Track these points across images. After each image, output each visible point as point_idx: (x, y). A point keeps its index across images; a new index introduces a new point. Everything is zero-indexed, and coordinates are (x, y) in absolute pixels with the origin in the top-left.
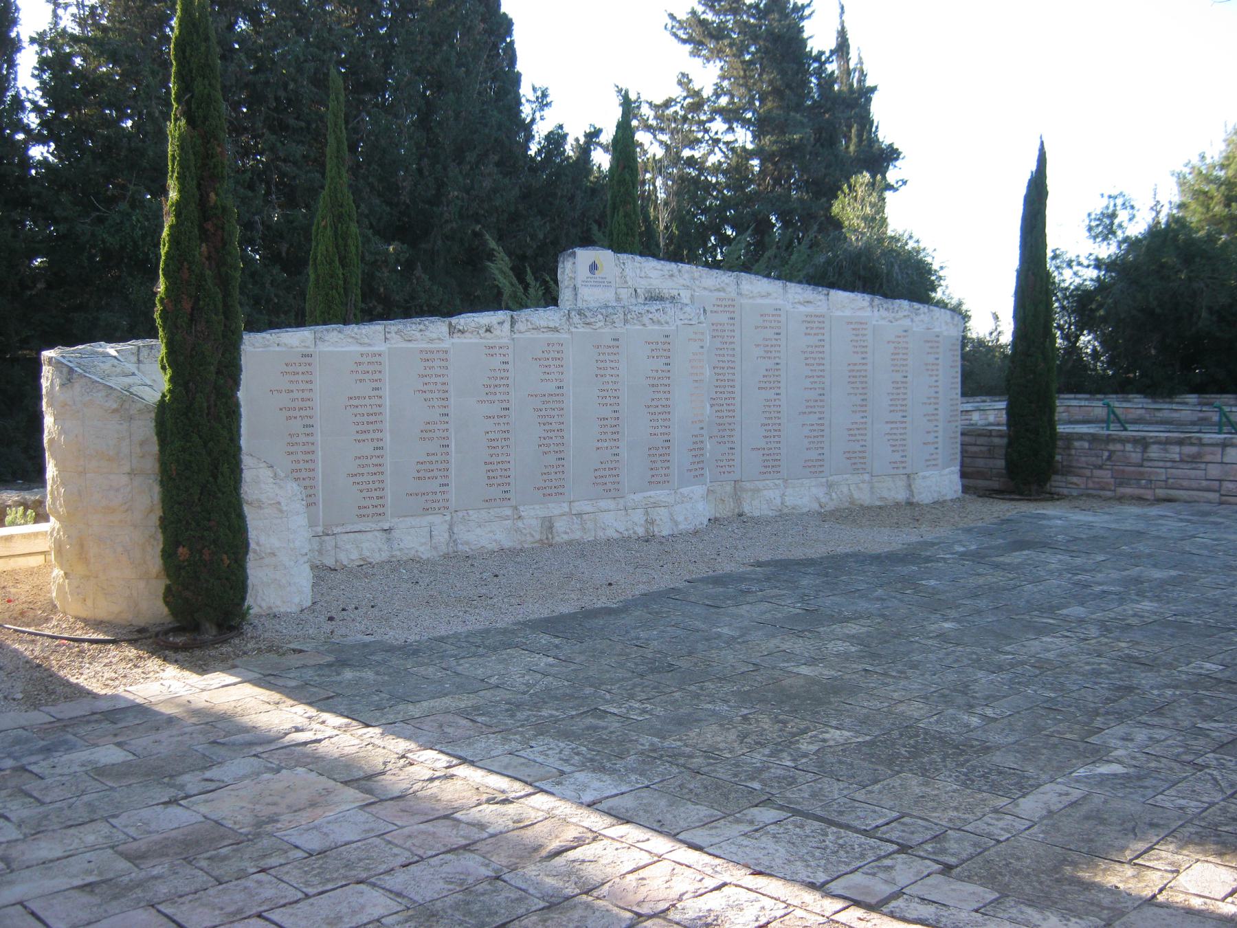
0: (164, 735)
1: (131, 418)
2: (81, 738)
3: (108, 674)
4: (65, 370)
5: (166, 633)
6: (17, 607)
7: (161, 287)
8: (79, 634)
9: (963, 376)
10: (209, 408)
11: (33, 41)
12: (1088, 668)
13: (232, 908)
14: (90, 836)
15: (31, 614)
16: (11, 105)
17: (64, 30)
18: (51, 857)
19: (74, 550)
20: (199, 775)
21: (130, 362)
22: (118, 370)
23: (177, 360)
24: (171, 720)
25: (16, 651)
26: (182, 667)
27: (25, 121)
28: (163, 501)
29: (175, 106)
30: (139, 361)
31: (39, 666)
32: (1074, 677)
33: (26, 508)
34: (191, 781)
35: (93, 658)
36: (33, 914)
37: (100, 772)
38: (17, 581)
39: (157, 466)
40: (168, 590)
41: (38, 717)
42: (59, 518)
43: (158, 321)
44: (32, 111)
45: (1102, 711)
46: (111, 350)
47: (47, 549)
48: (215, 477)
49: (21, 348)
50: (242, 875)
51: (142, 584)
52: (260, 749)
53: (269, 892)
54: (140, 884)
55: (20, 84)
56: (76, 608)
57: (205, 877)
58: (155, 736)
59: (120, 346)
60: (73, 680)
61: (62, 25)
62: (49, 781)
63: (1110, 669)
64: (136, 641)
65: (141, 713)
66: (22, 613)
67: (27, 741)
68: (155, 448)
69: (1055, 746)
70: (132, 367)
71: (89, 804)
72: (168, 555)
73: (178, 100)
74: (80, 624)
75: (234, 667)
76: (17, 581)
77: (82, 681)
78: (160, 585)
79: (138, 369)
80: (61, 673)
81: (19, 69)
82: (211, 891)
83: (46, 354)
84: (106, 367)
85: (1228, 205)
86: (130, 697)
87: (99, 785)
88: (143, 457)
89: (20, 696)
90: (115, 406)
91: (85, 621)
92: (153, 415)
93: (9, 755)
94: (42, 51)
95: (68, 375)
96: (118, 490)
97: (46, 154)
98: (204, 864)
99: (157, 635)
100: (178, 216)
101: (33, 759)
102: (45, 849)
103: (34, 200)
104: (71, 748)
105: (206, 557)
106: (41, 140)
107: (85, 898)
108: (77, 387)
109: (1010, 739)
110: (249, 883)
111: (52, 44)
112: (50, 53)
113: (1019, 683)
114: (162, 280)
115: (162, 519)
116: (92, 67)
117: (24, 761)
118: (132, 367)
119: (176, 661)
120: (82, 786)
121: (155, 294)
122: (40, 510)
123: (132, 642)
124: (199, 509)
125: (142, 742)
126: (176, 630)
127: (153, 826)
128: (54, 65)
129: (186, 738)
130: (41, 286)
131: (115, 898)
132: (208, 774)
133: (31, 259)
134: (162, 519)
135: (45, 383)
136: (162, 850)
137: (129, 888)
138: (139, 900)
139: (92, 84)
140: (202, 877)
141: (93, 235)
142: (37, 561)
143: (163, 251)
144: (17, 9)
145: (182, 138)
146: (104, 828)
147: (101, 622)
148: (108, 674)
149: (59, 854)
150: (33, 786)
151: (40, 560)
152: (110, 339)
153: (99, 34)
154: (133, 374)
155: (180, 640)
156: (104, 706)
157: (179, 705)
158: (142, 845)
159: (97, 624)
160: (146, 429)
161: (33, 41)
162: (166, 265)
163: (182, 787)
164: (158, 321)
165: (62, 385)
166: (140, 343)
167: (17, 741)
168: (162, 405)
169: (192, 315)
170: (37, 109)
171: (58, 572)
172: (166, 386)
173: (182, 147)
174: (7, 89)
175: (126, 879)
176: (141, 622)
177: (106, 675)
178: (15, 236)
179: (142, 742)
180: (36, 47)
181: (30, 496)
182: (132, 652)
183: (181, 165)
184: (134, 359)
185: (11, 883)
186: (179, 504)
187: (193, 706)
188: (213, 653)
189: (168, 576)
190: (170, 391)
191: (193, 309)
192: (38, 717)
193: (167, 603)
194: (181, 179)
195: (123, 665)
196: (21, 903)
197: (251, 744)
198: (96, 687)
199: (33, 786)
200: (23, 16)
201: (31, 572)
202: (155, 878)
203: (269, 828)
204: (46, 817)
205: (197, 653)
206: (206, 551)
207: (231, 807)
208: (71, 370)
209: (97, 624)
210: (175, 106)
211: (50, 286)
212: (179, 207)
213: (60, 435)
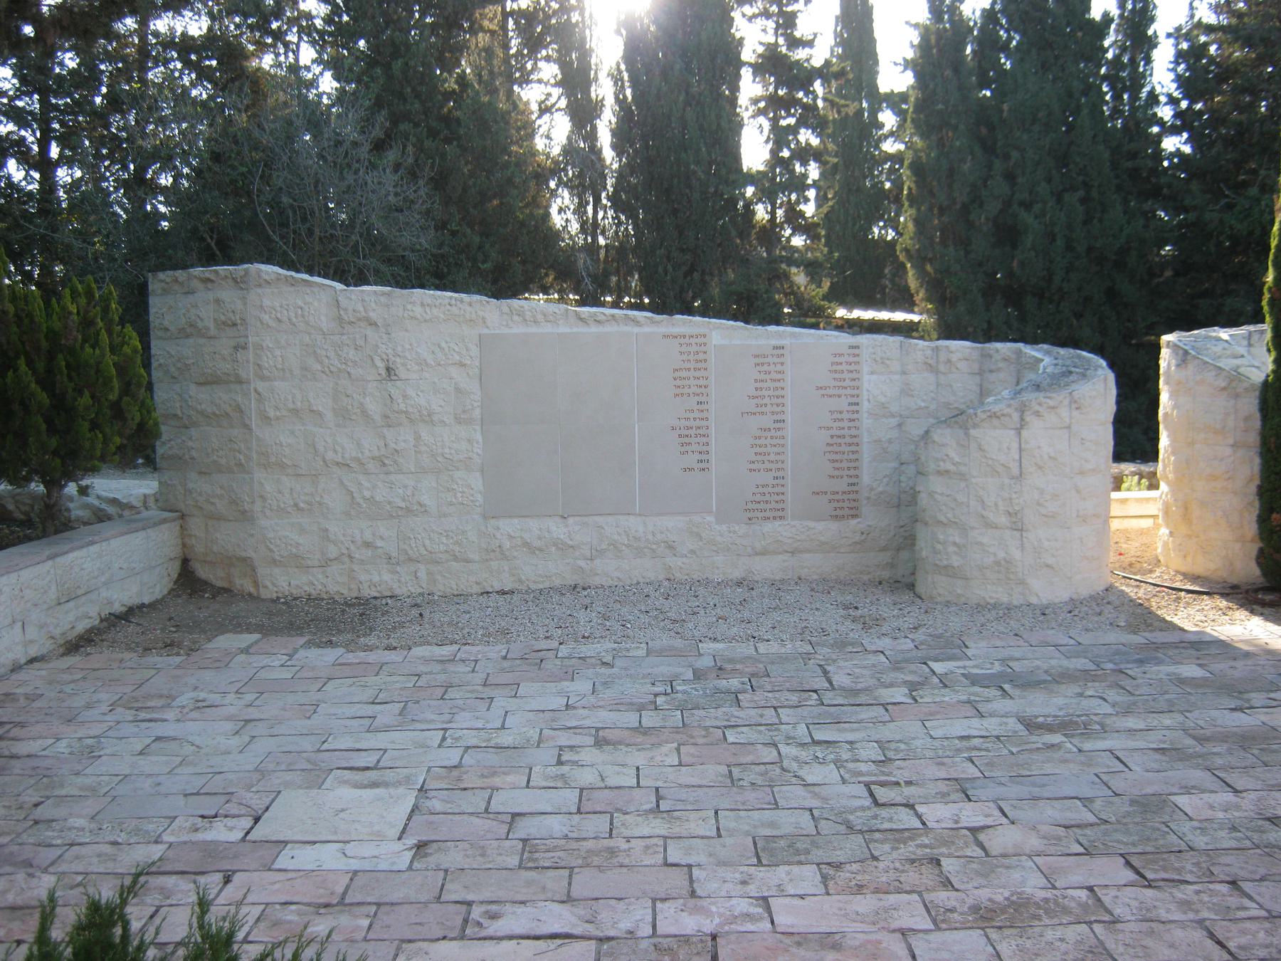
0: (1239, 664)
1: (1237, 396)
3: (1199, 617)
4: (1181, 352)
5: (1257, 591)
6: (1126, 560)
11: (1169, 35)
14: (1167, 721)
16: (1146, 100)
17: (1200, 22)
18: (1135, 727)
19: (1181, 513)
20: (1265, 695)
22: (1229, 352)
24: (1247, 655)
25: (1123, 591)
26: (1267, 619)
30: (1250, 345)
33: (1141, 477)
34: (1257, 698)
36: (1118, 758)
37: (1181, 681)
38: (1128, 539)
40: (1261, 551)
41: (1138, 639)
42: (1168, 483)
43: (1266, 309)
46: (1224, 334)
49: (1147, 334)
51: (1238, 546)
54: (1201, 756)
55: (1155, 80)
56: (1177, 563)
59: (1234, 331)
60: (1168, 618)
64: (1228, 595)
65: (1224, 648)
66: (1131, 565)
67: (1125, 653)
68: (1257, 424)
70: (1242, 351)
71: (1168, 701)
76: (1128, 539)
77: (1176, 620)
78: (1254, 548)
80: (1159, 613)
81: (1155, 64)
83: (1165, 338)
84: (1218, 349)
86: (1215, 634)
89: (1123, 624)
90: (1223, 384)
92: (1257, 393)
93: (1110, 661)
94: (1177, 45)
95: (1183, 356)
96: (1222, 460)
97: (1178, 146)
99: (1247, 592)
102: (1132, 722)
103: (1165, 190)
104: (1159, 662)
106: (1175, 130)
107: (1157, 756)
111: (1187, 36)
112: (1185, 46)
114: (1271, 270)
116: (1227, 54)
117: (1122, 666)
118: (1242, 351)
119: (1262, 614)
120: (1165, 688)
121: (1265, 283)
123: (1224, 595)
125: (1218, 667)
126: (1266, 590)
127: (1219, 722)
128: (1191, 56)
131: (1181, 760)
132: (1272, 695)
133: (1161, 247)
134: (1260, 487)
135: (1163, 364)
136: (1224, 738)
137: (1192, 756)
138: (1199, 765)
139: (1226, 71)
141: (1221, 221)
144: (1155, 7)
146: (1180, 718)
147: (1199, 577)
148: (1199, 617)
149: (1142, 726)
150: (1127, 683)
152: (1224, 326)
153: (1234, 21)
154: (1243, 356)
155: (1269, 598)
156: (1193, 638)
157: (1256, 646)
158: (1208, 733)
159: (1195, 578)
160: (1250, 405)
161: (1169, 35)
162: (1276, 257)
163: (1248, 701)
164: (1266, 309)
165: (1178, 366)
167: (1117, 653)
168: (1266, 384)
170: (1173, 101)
171: (1164, 531)
172: (1271, 367)
174: (1143, 86)
175: (1191, 751)
176: (1234, 580)
177: (1198, 618)
178: (1146, 226)
179: (1218, 667)
180: (1172, 41)
181: (1146, 468)
182: (1224, 603)
184: (1245, 343)
185: (1104, 739)
186: (1277, 474)
189: (1262, 539)
190: (1273, 371)
192: (1138, 639)
193: (1259, 564)
195: (1211, 613)
196: (1110, 751)
198: (1188, 626)
199: (1127, 683)
200: (1159, 13)
201: (1142, 532)
202: (1214, 754)
204: (1134, 704)
208: (1186, 352)
209: (1195, 578)
211: (1177, 274)
213: (1173, 408)
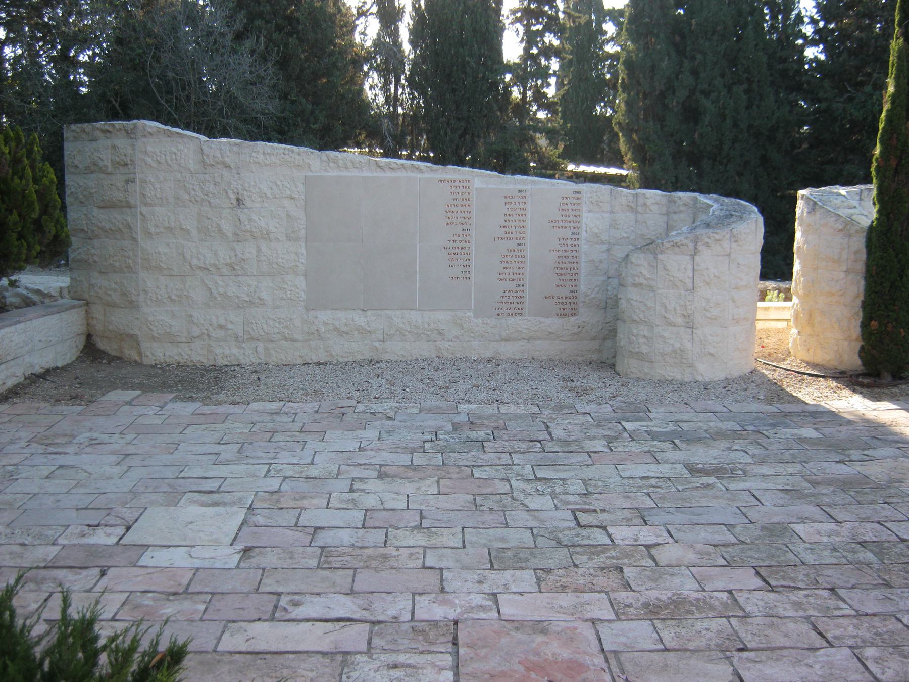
0: (843, 429)
1: (850, 236)
2: (795, 422)
3: (817, 393)
4: (811, 203)
5: (858, 376)
6: (767, 351)
7: (877, 151)
8: (802, 370)
10: (902, 231)
13: (864, 516)
14: (791, 469)
15: (775, 355)
16: (795, 20)
19: (807, 319)
20: (861, 452)
21: (854, 199)
22: (846, 204)
23: (883, 198)
24: (850, 422)
26: (864, 397)
27: (804, 31)
28: (865, 290)
29: (897, 29)
30: (861, 199)
31: (775, 384)
34: (855, 454)
35: (809, 383)
36: (754, 496)
37: (802, 440)
39: (864, 267)
40: (862, 348)
42: (799, 297)
43: (874, 173)
44: (808, 23)
46: (843, 191)
47: (789, 318)
48: (902, 278)
49: (788, 189)
50: (873, 502)
51: (846, 343)
52: (902, 445)
53: (887, 513)
55: (801, 6)
56: (802, 354)
57: (852, 499)
58: (838, 428)
59: (849, 189)
60: (795, 394)
62: (773, 439)
64: (837, 378)
65: (834, 417)
66: (770, 355)
67: (762, 419)
68: (864, 256)
70: (855, 203)
71: (792, 454)
72: (865, 325)
73: (900, 25)
74: (804, 365)
75: (898, 400)
77: (800, 396)
78: (858, 345)
79: (860, 204)
80: (788, 390)
82: (854, 506)
83: (801, 192)
84: (838, 202)
85: (297, 239)
86: (827, 406)
87: (801, 447)
88: (856, 261)
89: (762, 397)
90: (841, 227)
91: (808, 363)
92: (865, 234)
95: (813, 206)
97: (816, 54)
98: (853, 493)
99: (851, 376)
100: (893, 103)
101: (765, 428)
102: (765, 470)
105: (890, 329)
106: (814, 43)
107: (782, 495)
108: (818, 214)
110: (877, 507)
115: (863, 302)
117: (760, 428)
118: (855, 203)
120: (790, 445)
122: (789, 295)
123: (834, 378)
124: (887, 297)
125: (829, 430)
126: (864, 375)
127: (827, 471)
129: (857, 432)
130: (805, 146)
132: (866, 452)
133: (801, 127)
135: (798, 211)
136: (830, 482)
140: (849, 499)
142: (781, 325)
143: (881, 126)
145: (900, 51)
146: (799, 467)
148: (817, 393)
150: (763, 441)
151: (784, 324)
155: (866, 381)
156: (811, 409)
157: (856, 416)
158: (819, 478)
159: (815, 366)
160: (859, 243)
162: (882, 136)
163: (849, 456)
164: (874, 173)
165: (809, 213)
166: (863, 187)
167: (758, 418)
168: (871, 228)
169: (896, 169)
170: (813, 21)
171: (794, 331)
172: (875, 215)
173: (899, 57)
174: (792, 10)
176: (842, 368)
178: (790, 112)
179: (829, 430)
181: (783, 285)
182: (834, 384)
183: (897, 69)
184: (858, 197)
185: (746, 481)
187: (865, 417)
188: (886, 391)
189: (863, 339)
190: (877, 219)
191: (897, 165)
193: (860, 356)
194: (897, 79)
197: (897, 442)
198: (808, 400)
199: (763, 441)
201: (778, 331)
202: (823, 494)
203: (897, 485)
204: (768, 456)
205: (876, 390)
206: (890, 325)
207: (875, 471)
208: (815, 203)
209: (815, 366)
210: (897, 29)
211: (811, 146)
212: (894, 97)
213: (804, 244)
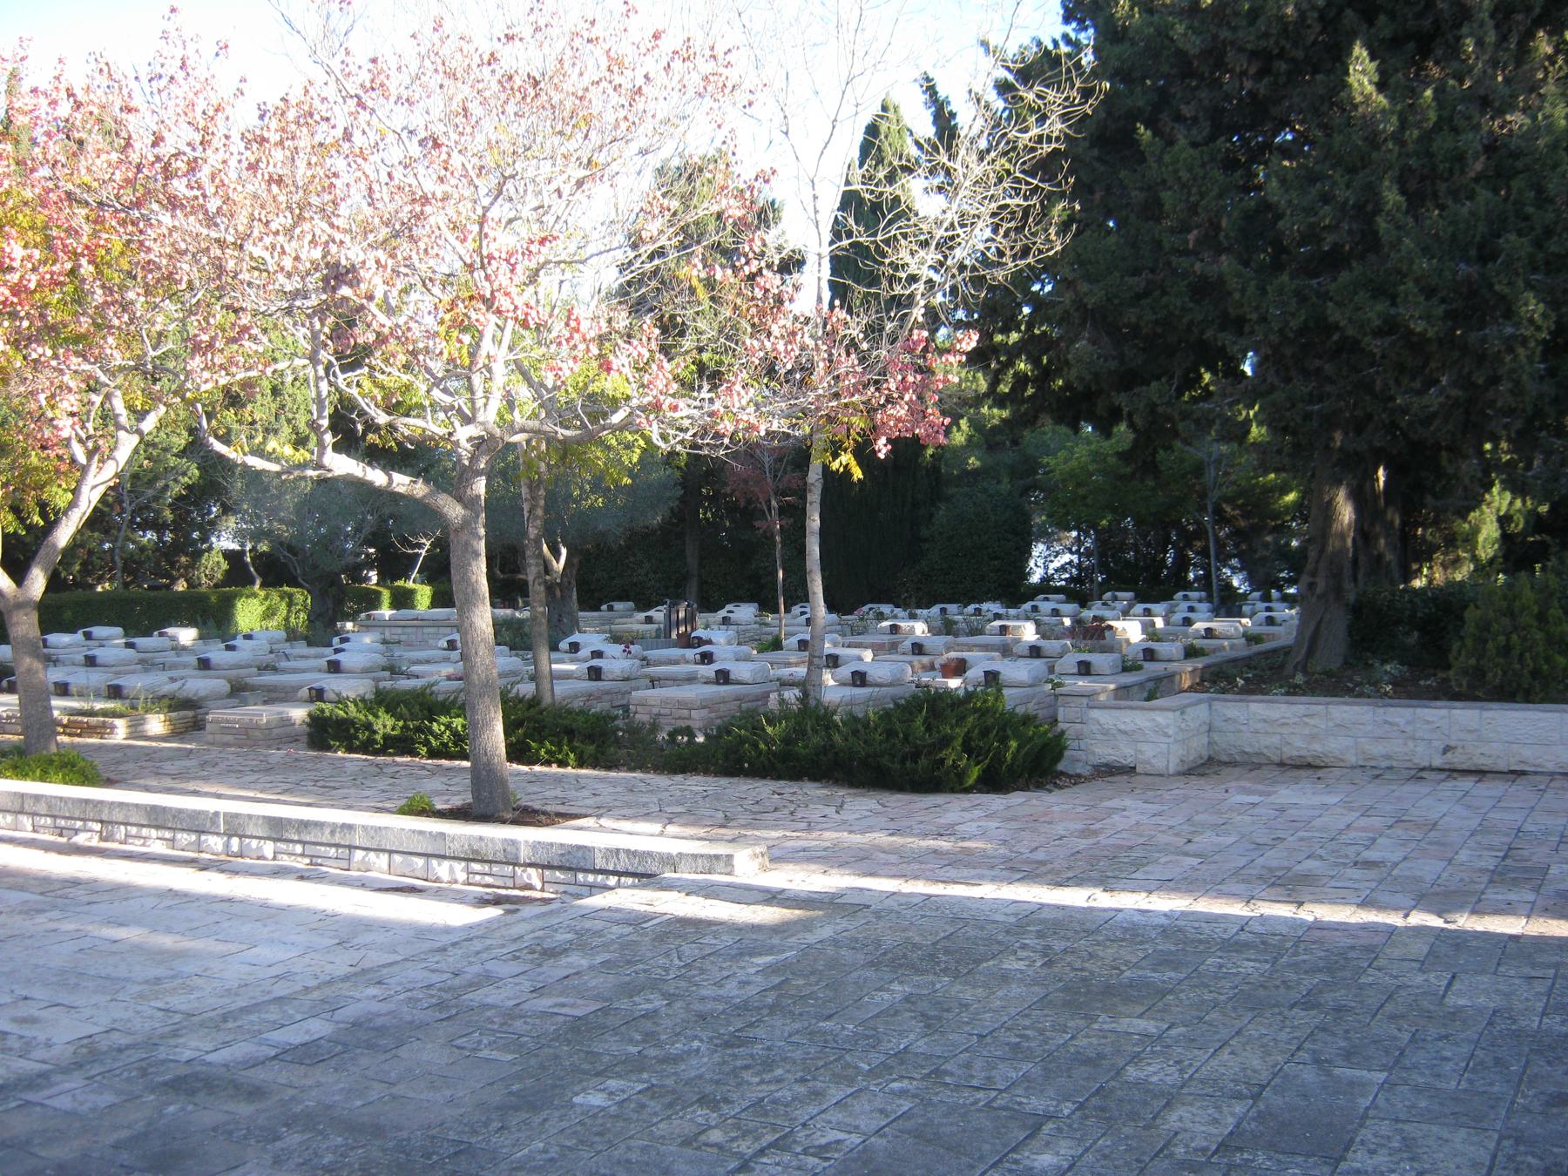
9: (449, 572)
12: (779, 1072)
32: (798, 1054)
45: (765, 1012)
61: (1324, 235)
63: (747, 1075)
69: (812, 973)
109: (855, 975)
113: (868, 1037)
